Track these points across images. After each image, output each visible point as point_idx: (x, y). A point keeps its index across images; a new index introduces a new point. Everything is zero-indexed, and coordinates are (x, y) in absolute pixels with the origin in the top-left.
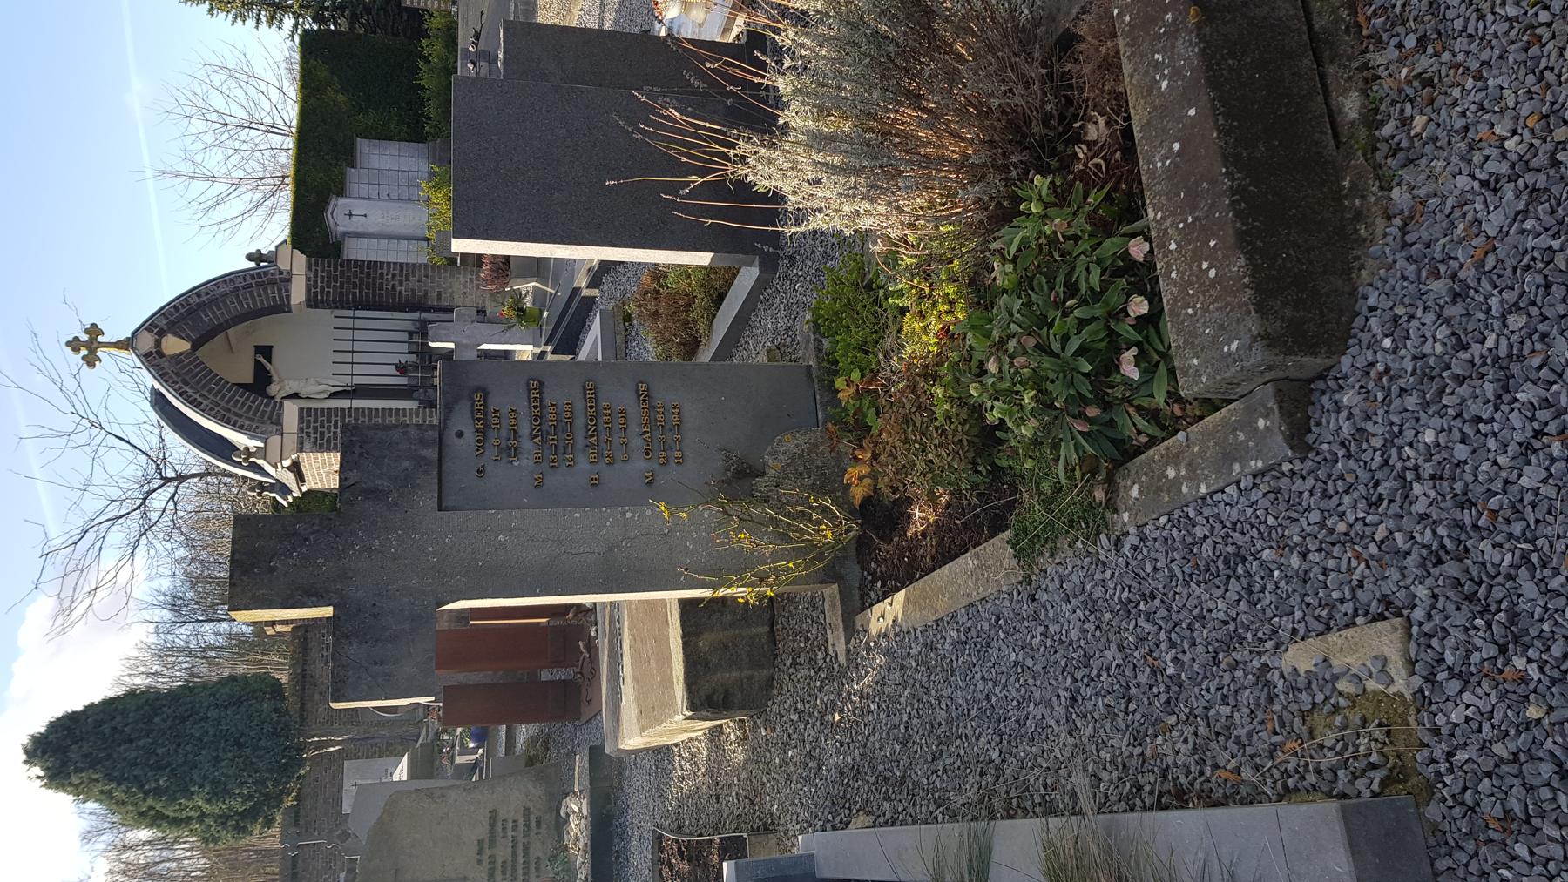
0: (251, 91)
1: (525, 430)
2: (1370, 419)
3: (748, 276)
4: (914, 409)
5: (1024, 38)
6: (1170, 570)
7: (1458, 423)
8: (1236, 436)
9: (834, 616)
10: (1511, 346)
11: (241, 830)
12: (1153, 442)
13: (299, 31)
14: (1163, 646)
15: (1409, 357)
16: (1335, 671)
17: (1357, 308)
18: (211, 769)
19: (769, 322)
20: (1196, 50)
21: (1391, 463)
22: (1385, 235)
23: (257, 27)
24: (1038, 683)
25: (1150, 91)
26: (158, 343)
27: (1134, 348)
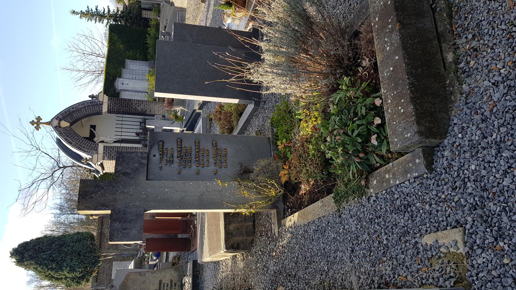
0: (92, 43)
1: (175, 155)
2: (454, 160)
3: (250, 107)
4: (303, 152)
6: (386, 209)
7: (483, 163)
9: (274, 220)
10: (501, 138)
11: (79, 283)
12: (381, 166)
13: (109, 24)
14: (383, 234)
16: (440, 245)
19: (256, 122)
21: (460, 175)
24: (341, 245)
25: (383, 50)
26: (59, 123)
27: (376, 135)
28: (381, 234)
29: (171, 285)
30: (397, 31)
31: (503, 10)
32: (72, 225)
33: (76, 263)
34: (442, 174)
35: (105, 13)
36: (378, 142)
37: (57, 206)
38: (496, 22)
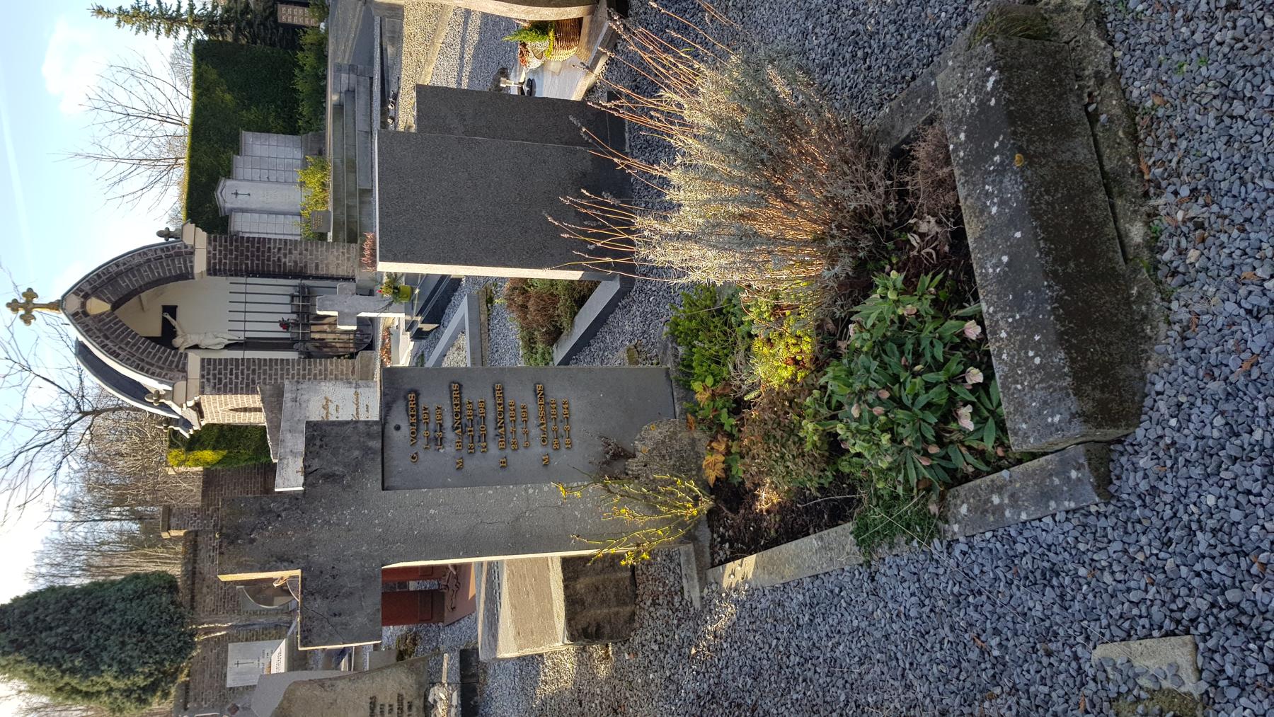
1: (448, 423)
2: (1161, 480)
5: (865, 146)
7: (1233, 492)
8: (1052, 481)
11: (142, 701)
12: (978, 474)
17: (1146, 391)
19: (628, 325)
20: (1021, 188)
21: (1178, 515)
22: (1167, 337)
23: (157, 37)
25: (982, 212)
26: (83, 305)
27: (969, 406)
28: (984, 632)
29: (401, 709)
31: (1266, 146)
32: (106, 547)
33: (135, 654)
34: (1135, 508)
35: (182, 11)
36: (976, 424)
37: (63, 502)
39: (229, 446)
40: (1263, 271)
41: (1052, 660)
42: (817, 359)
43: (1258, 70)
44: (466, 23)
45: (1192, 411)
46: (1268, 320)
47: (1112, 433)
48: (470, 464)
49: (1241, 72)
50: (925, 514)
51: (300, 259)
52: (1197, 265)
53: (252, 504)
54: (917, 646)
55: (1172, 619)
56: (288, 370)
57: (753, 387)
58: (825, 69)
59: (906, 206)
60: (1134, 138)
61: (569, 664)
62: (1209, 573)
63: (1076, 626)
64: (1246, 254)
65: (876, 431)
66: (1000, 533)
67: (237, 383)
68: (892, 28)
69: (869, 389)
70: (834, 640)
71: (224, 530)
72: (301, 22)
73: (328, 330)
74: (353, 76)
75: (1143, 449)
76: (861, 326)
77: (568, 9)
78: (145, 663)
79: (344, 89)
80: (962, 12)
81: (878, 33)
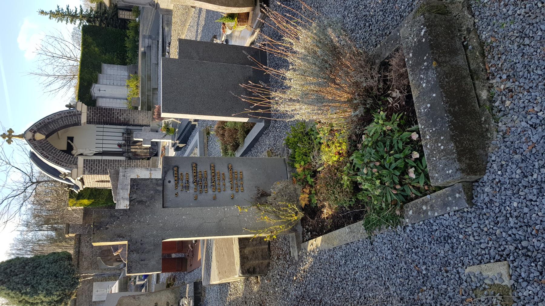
0: (62, 44)
1: (191, 180)
2: (494, 197)
5: (370, 61)
7: (525, 201)
8: (448, 198)
10: (542, 178)
12: (417, 197)
15: (507, 178)
16: (484, 277)
17: (488, 160)
18: (46, 285)
19: (267, 141)
22: (497, 137)
23: (66, 24)
26: (34, 136)
27: (413, 168)
28: (419, 264)
30: (433, 70)
31: (538, 56)
32: (41, 242)
33: (53, 286)
34: (483, 209)
35: (77, 13)
37: (23, 222)
38: (532, 67)
39: (95, 198)
40: (537, 109)
41: (448, 274)
42: (349, 152)
43: (535, 25)
44: (199, 17)
45: (508, 168)
46: (540, 129)
47: (474, 178)
48: (200, 197)
49: (528, 26)
50: (394, 215)
51: (127, 117)
52: (509, 107)
53: (107, 213)
54: (391, 271)
55: (499, 255)
56: (121, 164)
57: (321, 165)
58: (352, 31)
59: (387, 86)
60: (483, 55)
61: (241, 287)
62: (515, 235)
63: (458, 260)
64: (530, 102)
65: (374, 179)
66: (426, 222)
67: (99, 170)
68: (381, 13)
69: (371, 162)
70: (355, 271)
71: (95, 224)
72: (128, 18)
73: (138, 148)
74: (150, 40)
75: (487, 184)
76: (368, 136)
77: (243, 8)
78: (57, 290)
79: (147, 45)
80: (410, 5)
81: (375, 15)
